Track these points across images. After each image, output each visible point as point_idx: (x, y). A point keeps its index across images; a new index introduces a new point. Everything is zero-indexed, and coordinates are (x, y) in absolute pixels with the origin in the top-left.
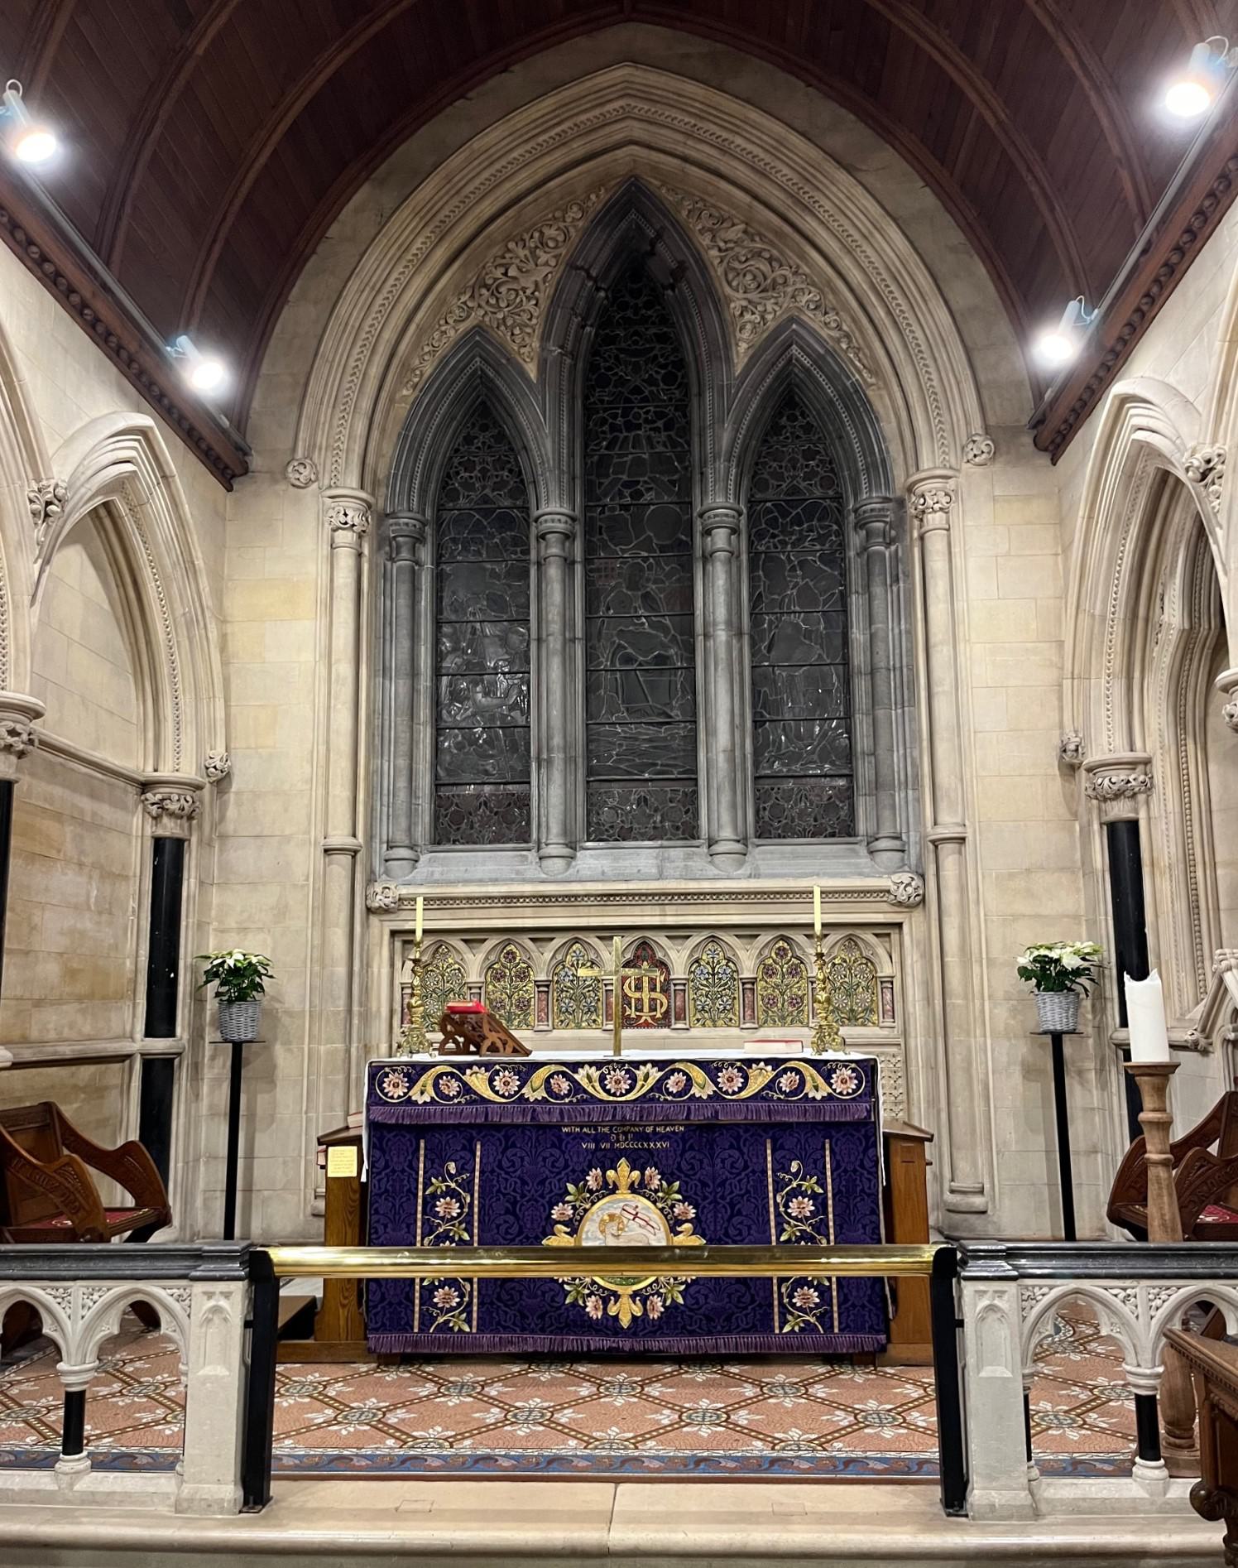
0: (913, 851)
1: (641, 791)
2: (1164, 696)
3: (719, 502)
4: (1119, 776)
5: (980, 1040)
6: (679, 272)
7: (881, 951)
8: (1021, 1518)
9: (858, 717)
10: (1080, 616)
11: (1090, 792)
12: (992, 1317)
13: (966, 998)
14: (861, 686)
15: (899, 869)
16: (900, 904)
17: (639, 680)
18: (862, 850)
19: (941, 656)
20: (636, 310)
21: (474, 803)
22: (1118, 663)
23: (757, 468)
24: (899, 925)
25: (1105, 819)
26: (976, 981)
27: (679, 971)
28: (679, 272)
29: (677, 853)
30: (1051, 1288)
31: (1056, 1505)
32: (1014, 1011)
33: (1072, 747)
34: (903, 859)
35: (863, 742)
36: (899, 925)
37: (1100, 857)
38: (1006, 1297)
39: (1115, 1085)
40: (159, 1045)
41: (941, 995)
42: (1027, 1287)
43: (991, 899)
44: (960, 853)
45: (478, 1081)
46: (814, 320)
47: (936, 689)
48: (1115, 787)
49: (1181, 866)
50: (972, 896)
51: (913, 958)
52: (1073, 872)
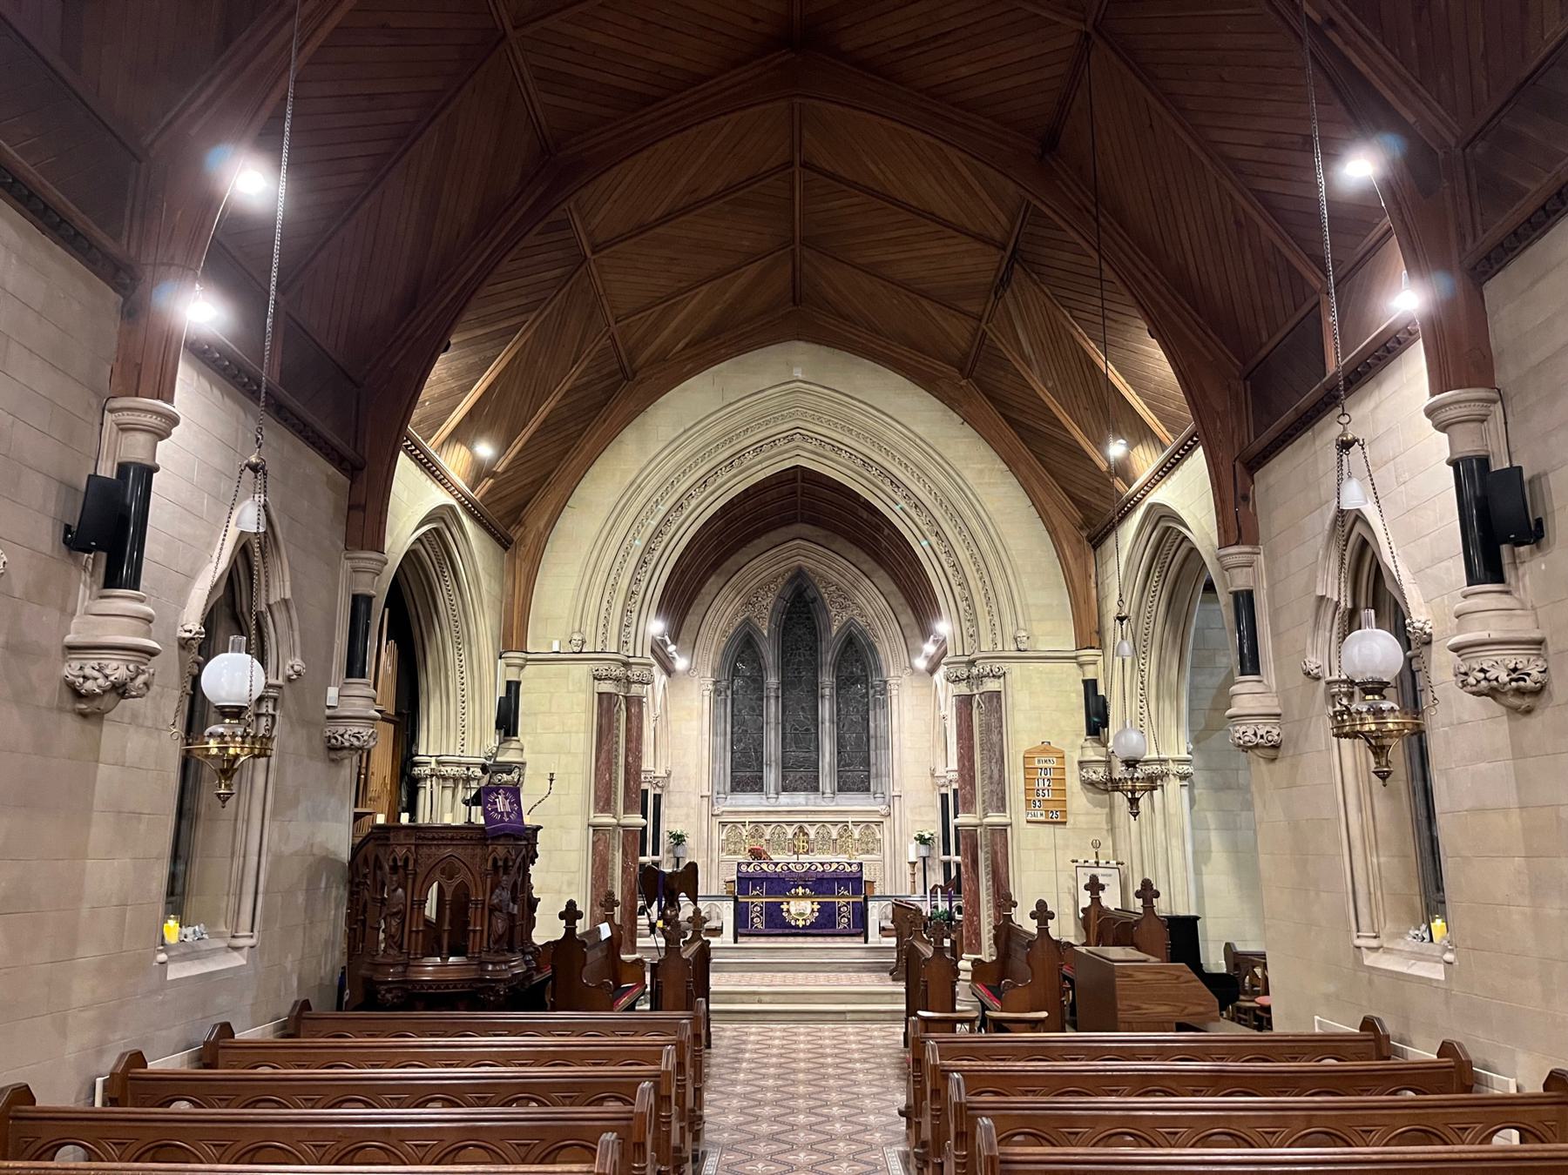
1: (800, 776)
3: (827, 680)
6: (814, 600)
17: (800, 738)
20: (800, 609)
21: (745, 776)
23: (838, 667)
27: (812, 837)
28: (814, 600)
29: (812, 796)
35: (873, 760)
40: (946, 858)
45: (764, 866)
46: (859, 619)
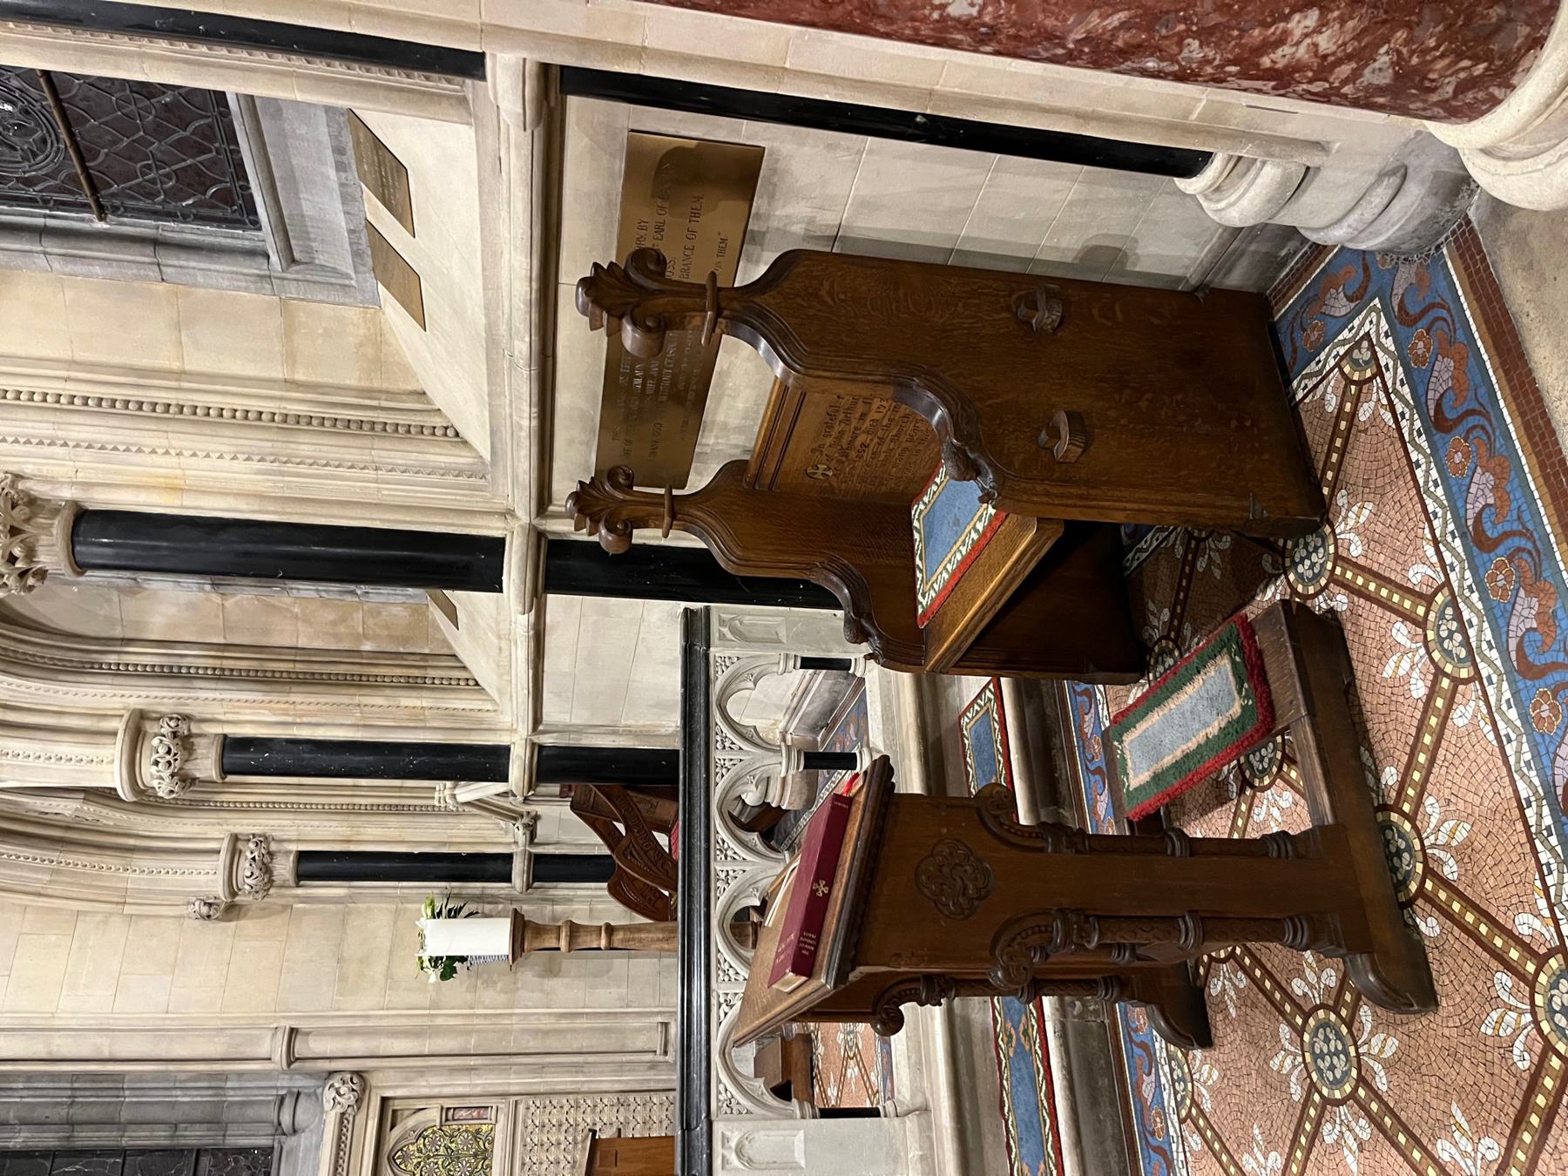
0: (300, 1083)
2: (160, 820)
4: (245, 868)
5: (514, 1020)
7: (411, 1122)
8: (930, 1128)
9: (124, 1142)
10: (49, 892)
11: (259, 896)
12: (748, 1150)
13: (469, 1033)
14: (87, 1138)
15: (316, 1097)
16: (359, 1101)
18: (290, 1142)
19: (64, 1046)
22: (111, 861)
24: (384, 1100)
25: (292, 883)
26: (453, 1022)
30: (719, 1081)
31: (916, 1090)
32: (489, 983)
33: (205, 910)
34: (309, 1095)
36: (384, 1100)
37: (336, 889)
38: (728, 1134)
39: (566, 892)
41: (464, 1059)
42: (719, 1108)
43: (364, 1003)
44: (308, 1034)
47: (106, 1054)
48: (257, 873)
49: (352, 818)
50: (359, 1023)
51: (423, 1086)
52: (349, 913)
